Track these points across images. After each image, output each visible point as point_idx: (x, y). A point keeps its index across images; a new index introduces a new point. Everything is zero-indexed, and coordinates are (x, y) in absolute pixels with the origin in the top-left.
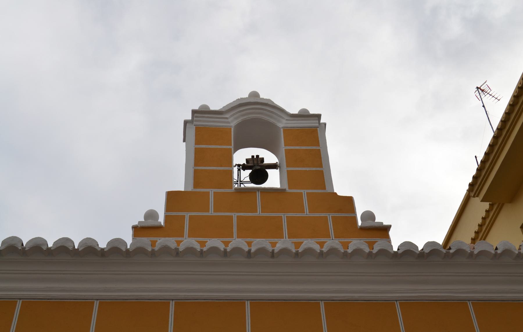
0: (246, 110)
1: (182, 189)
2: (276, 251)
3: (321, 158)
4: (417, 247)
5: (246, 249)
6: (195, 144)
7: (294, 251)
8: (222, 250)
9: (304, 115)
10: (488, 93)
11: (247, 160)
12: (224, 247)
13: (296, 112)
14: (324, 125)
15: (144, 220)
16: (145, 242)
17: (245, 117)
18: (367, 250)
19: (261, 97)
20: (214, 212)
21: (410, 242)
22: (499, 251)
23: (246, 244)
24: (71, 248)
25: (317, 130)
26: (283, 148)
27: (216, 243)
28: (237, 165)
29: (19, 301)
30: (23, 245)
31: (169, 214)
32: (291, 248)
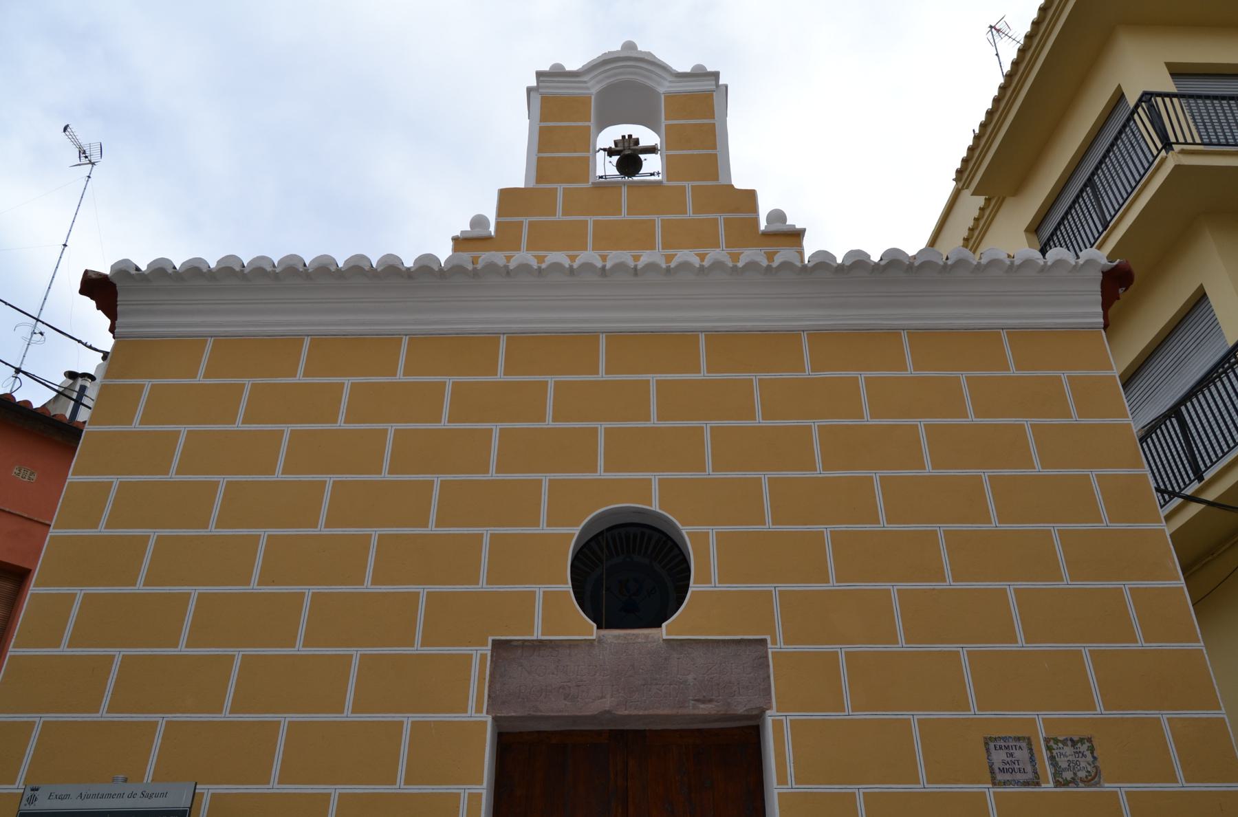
0: (622, 67)
1: (521, 185)
2: (639, 267)
3: (715, 136)
4: (834, 258)
5: (764, 263)
6: (541, 122)
7: (664, 266)
8: (567, 266)
9: (700, 74)
10: (1006, 35)
11: (616, 143)
12: (569, 262)
13: (688, 70)
14: (725, 88)
15: (469, 229)
16: (466, 258)
17: (612, 80)
18: (764, 263)
19: (639, 49)
20: (563, 215)
21: (826, 252)
22: (949, 262)
23: (600, 258)
24: (367, 268)
25: (712, 95)
26: (664, 122)
27: (559, 257)
28: (601, 149)
29: (306, 337)
30: (305, 265)
31: (502, 219)
32: (660, 263)
